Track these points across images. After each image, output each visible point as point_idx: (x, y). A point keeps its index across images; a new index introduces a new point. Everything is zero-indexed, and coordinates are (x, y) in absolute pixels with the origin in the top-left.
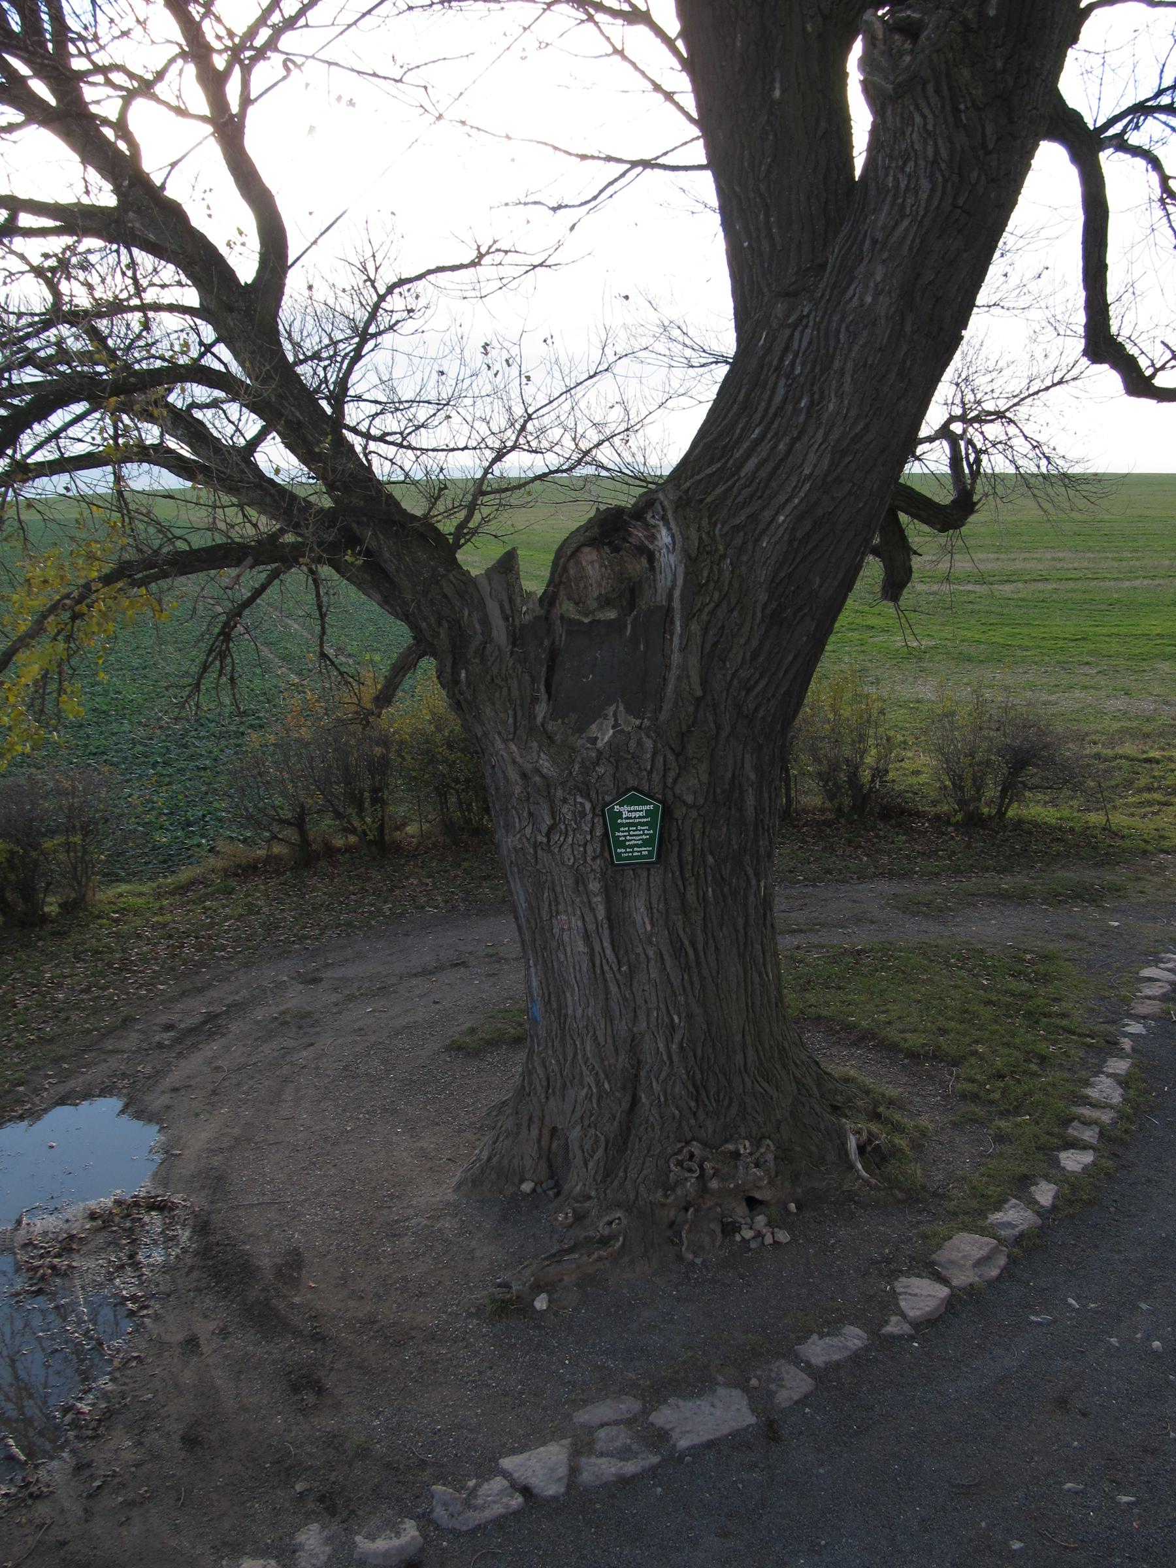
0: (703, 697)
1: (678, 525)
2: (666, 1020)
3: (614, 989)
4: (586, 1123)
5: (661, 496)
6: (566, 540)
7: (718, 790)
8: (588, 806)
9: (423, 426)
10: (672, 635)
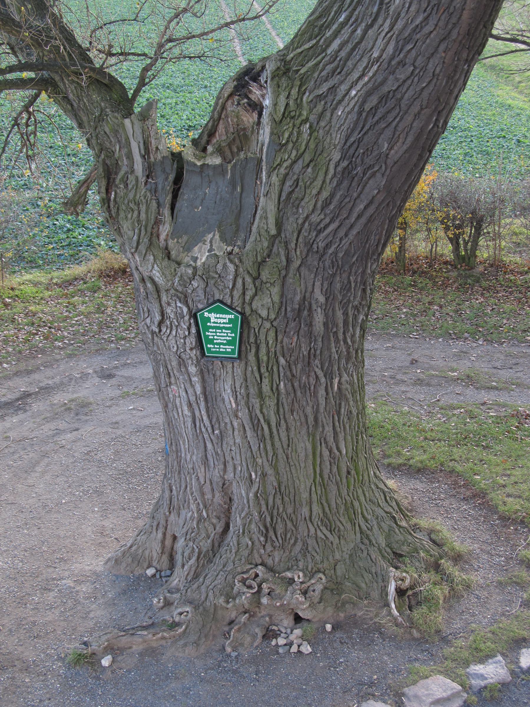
2: (246, 475)
3: (209, 446)
4: (188, 537)
7: (289, 309)
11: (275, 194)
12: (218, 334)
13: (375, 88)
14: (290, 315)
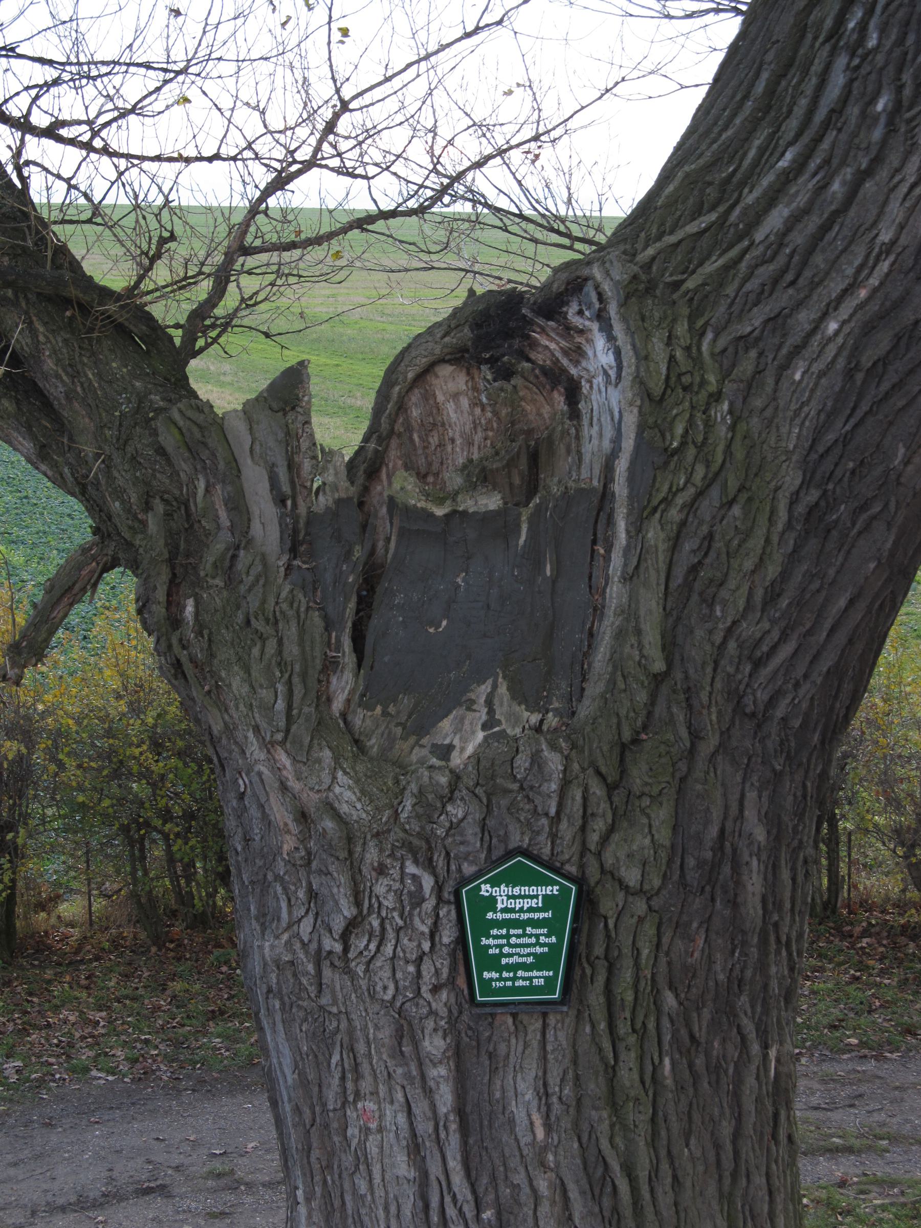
0: (666, 674)
1: (628, 330)
5: (597, 272)
6: (409, 346)
7: (691, 862)
8: (428, 882)
9: (133, 111)
10: (609, 549)
11: (658, 571)
12: (513, 940)
13: (883, 316)
14: (693, 877)
